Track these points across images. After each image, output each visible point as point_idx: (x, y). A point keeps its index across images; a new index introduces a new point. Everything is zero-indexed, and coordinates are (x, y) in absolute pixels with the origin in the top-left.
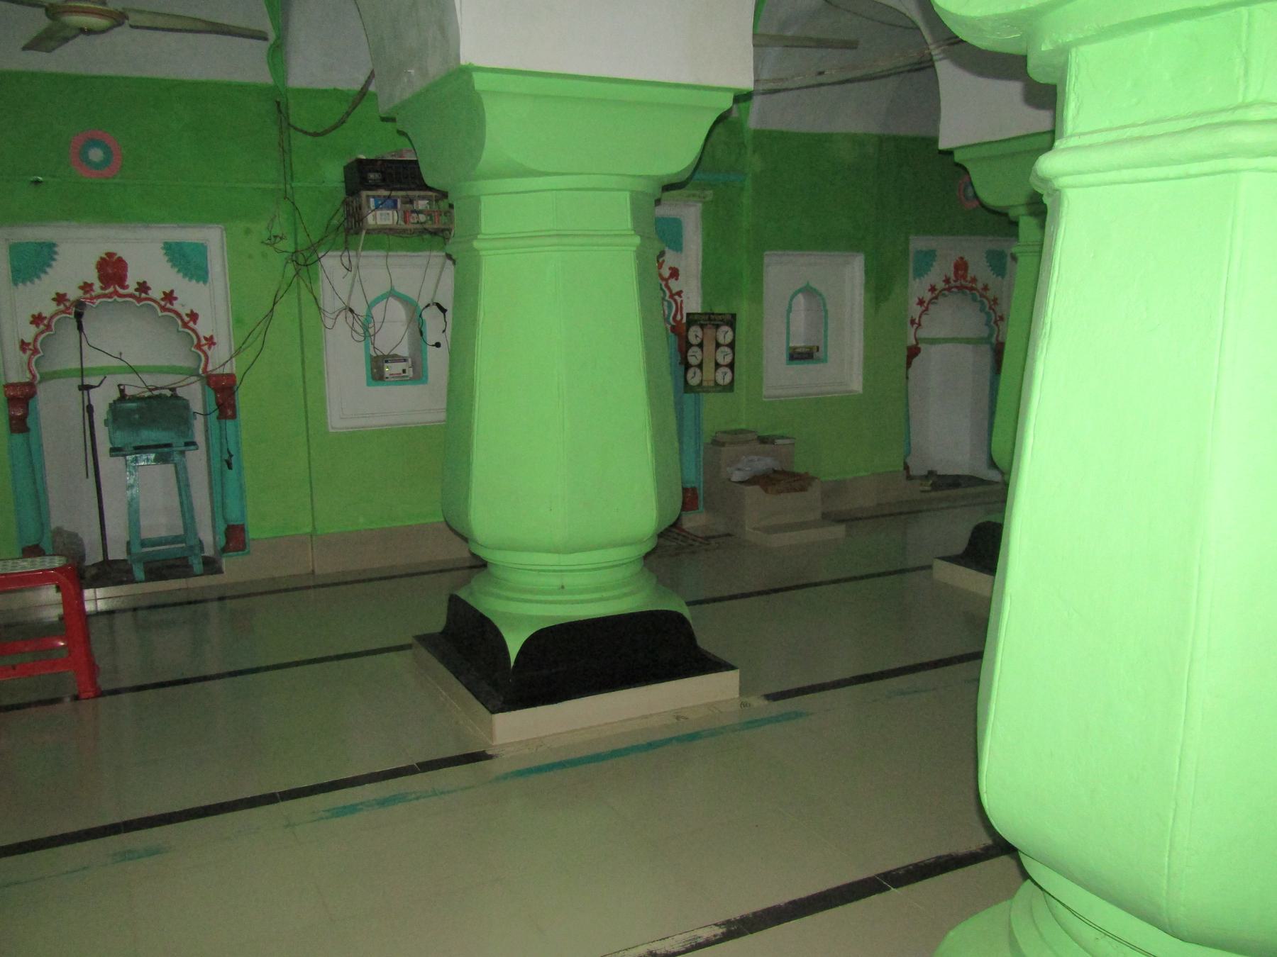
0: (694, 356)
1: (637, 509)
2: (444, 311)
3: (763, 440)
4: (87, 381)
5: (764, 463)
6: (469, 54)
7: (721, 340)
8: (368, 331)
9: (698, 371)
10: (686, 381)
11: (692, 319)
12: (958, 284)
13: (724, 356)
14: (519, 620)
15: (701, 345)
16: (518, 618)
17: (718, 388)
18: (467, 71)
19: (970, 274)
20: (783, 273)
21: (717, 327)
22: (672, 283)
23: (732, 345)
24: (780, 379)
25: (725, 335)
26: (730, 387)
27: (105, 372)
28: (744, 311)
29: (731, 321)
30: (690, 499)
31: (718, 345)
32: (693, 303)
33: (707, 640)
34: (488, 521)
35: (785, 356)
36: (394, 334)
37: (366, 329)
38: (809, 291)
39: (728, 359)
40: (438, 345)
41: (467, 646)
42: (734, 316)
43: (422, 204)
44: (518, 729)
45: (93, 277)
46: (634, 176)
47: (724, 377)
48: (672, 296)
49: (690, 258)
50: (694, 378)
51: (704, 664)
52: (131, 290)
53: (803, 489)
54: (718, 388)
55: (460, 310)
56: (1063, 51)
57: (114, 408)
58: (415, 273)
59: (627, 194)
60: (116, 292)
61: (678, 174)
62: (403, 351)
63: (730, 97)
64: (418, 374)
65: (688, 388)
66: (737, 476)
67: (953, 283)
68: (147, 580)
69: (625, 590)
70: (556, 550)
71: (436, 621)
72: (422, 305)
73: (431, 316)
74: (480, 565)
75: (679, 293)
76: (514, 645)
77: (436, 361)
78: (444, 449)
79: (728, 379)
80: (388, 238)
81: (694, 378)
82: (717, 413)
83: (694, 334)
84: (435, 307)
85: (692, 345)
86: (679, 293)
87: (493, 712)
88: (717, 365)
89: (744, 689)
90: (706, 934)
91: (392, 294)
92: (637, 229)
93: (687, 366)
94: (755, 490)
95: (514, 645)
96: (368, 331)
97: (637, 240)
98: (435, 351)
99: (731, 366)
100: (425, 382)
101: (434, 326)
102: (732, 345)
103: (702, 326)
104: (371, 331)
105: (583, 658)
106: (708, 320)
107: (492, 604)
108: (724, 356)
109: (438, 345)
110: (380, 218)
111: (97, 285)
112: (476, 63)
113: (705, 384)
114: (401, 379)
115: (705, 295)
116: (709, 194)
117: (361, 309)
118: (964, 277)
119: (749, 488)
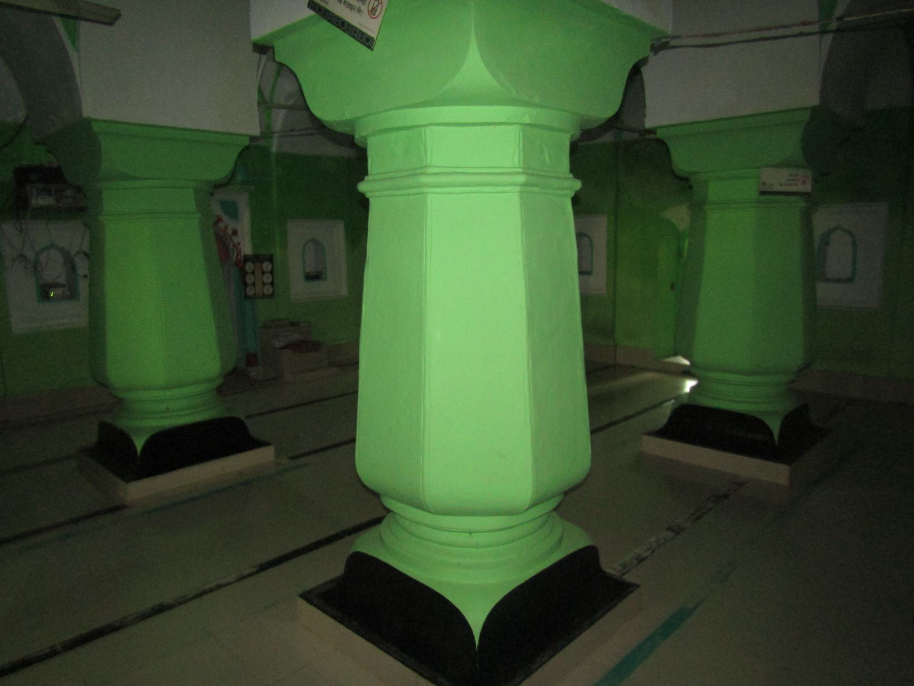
0: (249, 279)
1: (206, 359)
3: (293, 324)
5: (296, 337)
6: (88, 110)
7: (265, 269)
8: (36, 268)
10: (246, 294)
11: (247, 259)
13: (267, 279)
15: (253, 273)
17: (264, 296)
20: (298, 232)
21: (262, 262)
22: (234, 238)
23: (272, 272)
24: (299, 289)
25: (267, 266)
26: (272, 295)
28: (278, 252)
29: (271, 259)
30: (251, 359)
31: (263, 273)
32: (247, 249)
33: (255, 429)
34: (119, 372)
36: (55, 271)
37: (35, 267)
38: (314, 241)
39: (270, 280)
41: (117, 454)
43: (69, 193)
47: (268, 290)
48: (234, 245)
49: (244, 224)
50: (250, 291)
51: (253, 444)
54: (264, 296)
55: (94, 254)
56: (365, 138)
58: (68, 235)
59: (191, 190)
62: (62, 280)
64: (73, 294)
65: (246, 297)
66: (278, 344)
70: (163, 388)
71: (91, 437)
72: (73, 253)
74: (120, 402)
75: (239, 244)
76: (139, 444)
77: (83, 287)
78: (93, 336)
79: (271, 291)
80: (42, 213)
81: (250, 291)
83: (249, 267)
88: (264, 284)
89: (278, 453)
90: (248, 572)
91: (52, 246)
92: (527, 170)
93: (245, 284)
95: (139, 444)
96: (36, 268)
97: (199, 215)
98: (83, 278)
99: (272, 284)
100: (39, 301)
101: (82, 267)
102: (272, 272)
103: (254, 263)
104: (39, 269)
105: (179, 447)
106: (257, 258)
107: (124, 423)
108: (267, 279)
110: (40, 201)
112: (93, 117)
114: (61, 298)
115: (254, 245)
117: (30, 255)
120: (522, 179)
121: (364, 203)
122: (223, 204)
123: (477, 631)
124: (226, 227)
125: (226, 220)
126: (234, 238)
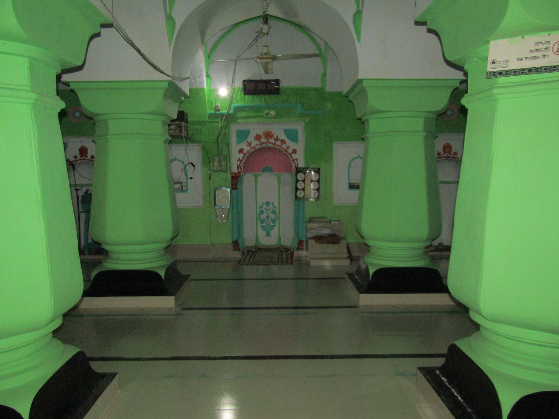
2: (194, 166)
4: (77, 188)
9: (302, 192)
12: (446, 155)
14: (374, 265)
15: (304, 181)
16: (375, 263)
18: (361, 81)
19: (453, 150)
22: (293, 155)
23: (318, 181)
27: (82, 186)
28: (323, 166)
35: (347, 186)
40: (191, 178)
42: (319, 169)
44: (369, 300)
45: (441, 150)
46: (430, 112)
52: (89, 158)
53: (337, 243)
57: (83, 197)
60: (84, 159)
61: (442, 109)
63: (459, 82)
67: (442, 155)
68: (89, 255)
69: (418, 259)
73: (189, 168)
76: (162, 274)
82: (310, 211)
84: (191, 165)
85: (299, 181)
86: (297, 160)
87: (361, 292)
92: (425, 131)
93: (297, 189)
94: (313, 241)
109: (191, 178)
111: (79, 156)
113: (306, 197)
116: (308, 119)
118: (449, 152)
119: (311, 240)
120: (424, 134)
121: (464, 111)
122: (286, 132)
123: (163, 278)
124: (288, 148)
125: (289, 143)
126: (293, 155)
